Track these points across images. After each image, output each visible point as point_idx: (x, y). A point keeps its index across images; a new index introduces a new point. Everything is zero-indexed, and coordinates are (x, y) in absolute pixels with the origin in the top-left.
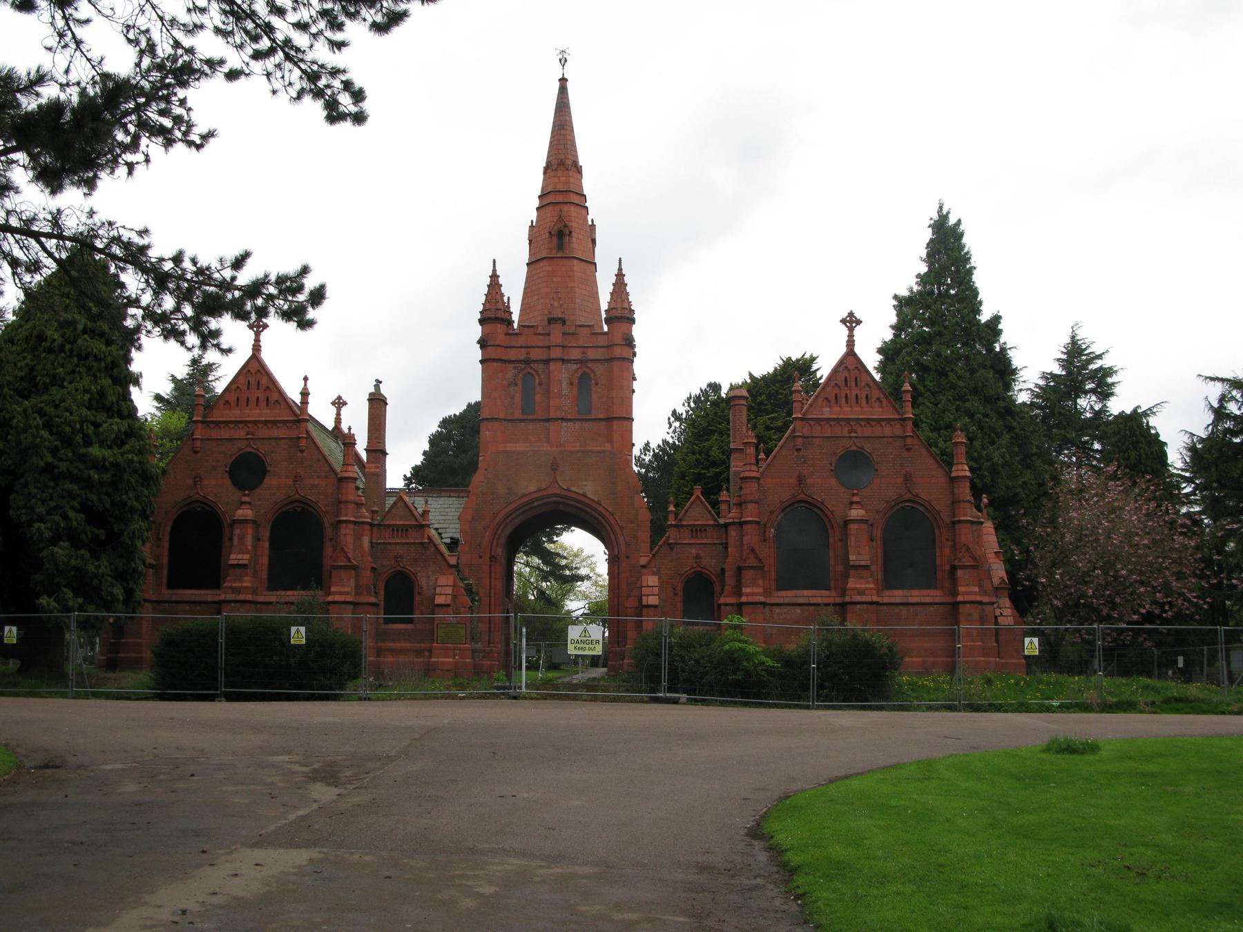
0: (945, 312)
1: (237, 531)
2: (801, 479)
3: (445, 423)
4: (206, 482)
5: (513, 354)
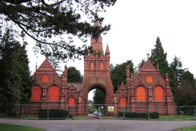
0: (158, 54)
1: (44, 90)
2: (141, 81)
3: (78, 71)
4: (38, 81)
5: (89, 60)
